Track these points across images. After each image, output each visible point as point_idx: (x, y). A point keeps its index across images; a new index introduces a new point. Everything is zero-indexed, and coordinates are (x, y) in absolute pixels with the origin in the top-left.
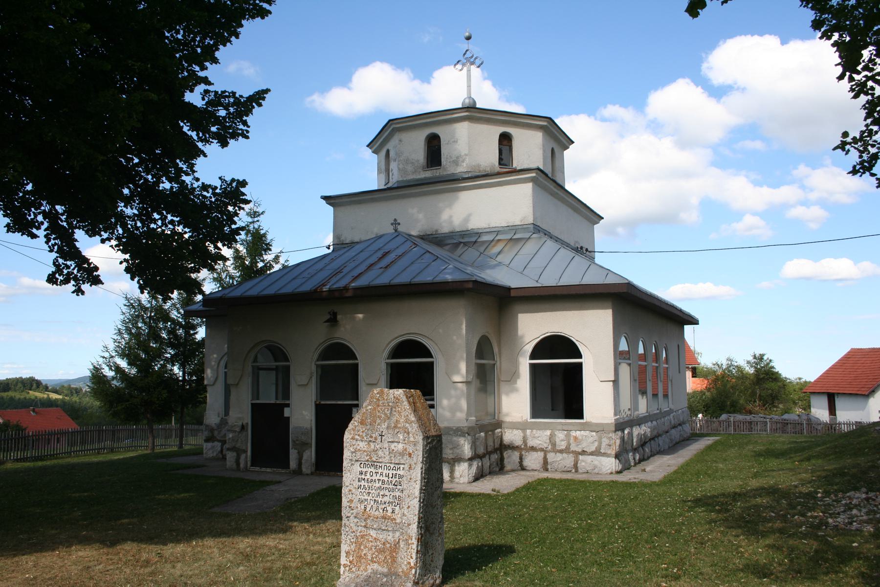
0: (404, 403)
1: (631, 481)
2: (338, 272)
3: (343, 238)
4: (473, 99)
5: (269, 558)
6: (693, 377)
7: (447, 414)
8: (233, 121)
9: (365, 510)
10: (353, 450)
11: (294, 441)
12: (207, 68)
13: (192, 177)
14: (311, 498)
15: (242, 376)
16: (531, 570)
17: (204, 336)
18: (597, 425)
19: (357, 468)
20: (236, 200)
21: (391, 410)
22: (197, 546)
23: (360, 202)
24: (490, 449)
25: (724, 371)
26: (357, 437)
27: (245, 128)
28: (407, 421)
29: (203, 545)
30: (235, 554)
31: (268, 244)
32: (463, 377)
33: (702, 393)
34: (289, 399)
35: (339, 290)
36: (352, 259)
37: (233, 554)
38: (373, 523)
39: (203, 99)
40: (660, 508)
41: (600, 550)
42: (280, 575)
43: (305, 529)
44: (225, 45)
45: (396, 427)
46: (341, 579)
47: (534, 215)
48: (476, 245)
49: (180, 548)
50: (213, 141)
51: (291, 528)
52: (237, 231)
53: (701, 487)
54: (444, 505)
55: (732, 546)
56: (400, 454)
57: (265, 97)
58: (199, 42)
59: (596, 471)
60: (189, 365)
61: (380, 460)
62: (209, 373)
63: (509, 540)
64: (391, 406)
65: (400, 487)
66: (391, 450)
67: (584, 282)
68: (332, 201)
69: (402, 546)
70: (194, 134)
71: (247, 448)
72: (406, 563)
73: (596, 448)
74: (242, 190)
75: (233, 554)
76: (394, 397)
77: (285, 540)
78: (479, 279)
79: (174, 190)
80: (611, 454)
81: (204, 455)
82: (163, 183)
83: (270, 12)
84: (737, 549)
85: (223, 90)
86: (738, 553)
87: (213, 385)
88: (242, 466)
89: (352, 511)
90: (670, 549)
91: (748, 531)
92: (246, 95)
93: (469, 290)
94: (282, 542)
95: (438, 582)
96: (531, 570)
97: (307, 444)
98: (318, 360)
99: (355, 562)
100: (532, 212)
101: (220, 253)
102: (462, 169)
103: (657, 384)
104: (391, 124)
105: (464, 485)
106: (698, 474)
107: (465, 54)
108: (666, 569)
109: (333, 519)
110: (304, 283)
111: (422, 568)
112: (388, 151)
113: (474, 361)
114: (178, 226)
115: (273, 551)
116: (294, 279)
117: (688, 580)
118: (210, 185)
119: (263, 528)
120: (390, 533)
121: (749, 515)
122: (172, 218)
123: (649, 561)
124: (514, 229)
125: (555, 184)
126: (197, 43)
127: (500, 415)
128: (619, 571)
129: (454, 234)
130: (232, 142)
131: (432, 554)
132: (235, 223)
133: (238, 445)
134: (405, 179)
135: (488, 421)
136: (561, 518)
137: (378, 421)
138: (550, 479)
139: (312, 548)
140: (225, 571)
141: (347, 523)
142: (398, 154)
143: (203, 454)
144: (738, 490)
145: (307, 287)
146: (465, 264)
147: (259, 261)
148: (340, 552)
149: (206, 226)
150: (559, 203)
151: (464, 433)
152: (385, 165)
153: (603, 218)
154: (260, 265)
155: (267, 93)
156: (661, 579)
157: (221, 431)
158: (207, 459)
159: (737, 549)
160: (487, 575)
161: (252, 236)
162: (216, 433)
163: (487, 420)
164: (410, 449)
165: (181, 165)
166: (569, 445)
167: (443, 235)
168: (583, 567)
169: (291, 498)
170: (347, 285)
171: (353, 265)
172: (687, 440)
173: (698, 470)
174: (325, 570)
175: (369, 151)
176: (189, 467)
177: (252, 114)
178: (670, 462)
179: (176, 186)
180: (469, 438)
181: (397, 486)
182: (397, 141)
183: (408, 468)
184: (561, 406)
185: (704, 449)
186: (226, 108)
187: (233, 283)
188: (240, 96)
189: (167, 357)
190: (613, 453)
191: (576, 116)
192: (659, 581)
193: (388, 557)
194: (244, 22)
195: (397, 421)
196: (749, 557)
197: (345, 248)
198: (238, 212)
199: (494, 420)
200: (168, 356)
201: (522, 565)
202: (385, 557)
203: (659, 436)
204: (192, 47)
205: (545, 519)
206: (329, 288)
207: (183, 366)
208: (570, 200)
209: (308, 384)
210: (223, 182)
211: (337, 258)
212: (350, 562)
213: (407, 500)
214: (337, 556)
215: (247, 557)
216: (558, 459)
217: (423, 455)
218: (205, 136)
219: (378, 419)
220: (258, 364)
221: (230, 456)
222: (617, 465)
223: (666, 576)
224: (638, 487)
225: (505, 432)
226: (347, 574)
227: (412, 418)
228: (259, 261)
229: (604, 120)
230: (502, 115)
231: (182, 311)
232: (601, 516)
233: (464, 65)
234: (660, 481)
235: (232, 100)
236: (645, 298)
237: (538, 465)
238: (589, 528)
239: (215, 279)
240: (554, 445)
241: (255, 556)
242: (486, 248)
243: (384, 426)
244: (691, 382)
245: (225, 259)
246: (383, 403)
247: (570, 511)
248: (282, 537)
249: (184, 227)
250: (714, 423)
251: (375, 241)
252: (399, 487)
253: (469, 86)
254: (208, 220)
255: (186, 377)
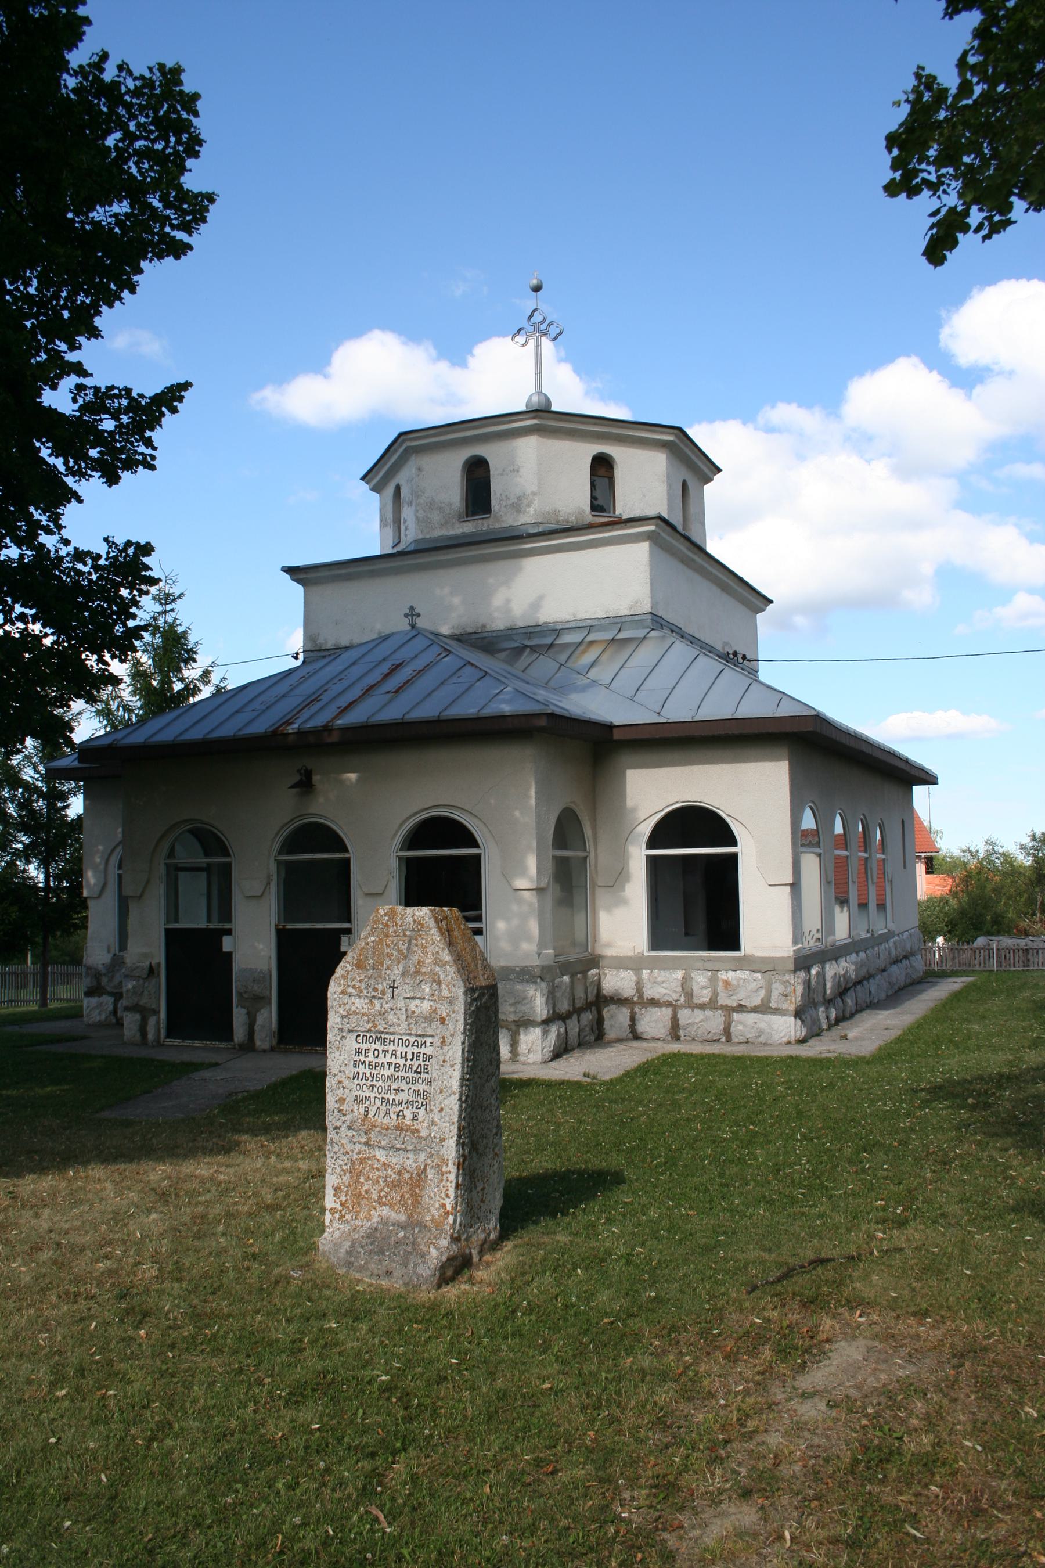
0: (432, 932)
1: (823, 1056)
2: (313, 699)
3: (321, 640)
4: (545, 395)
5: (202, 1199)
6: (927, 873)
7: (505, 945)
8: (127, 439)
9: (366, 1116)
10: (344, 1013)
11: (240, 994)
12: (80, 345)
13: (57, 537)
14: (270, 1093)
15: (147, 883)
16: (653, 1214)
17: (81, 811)
18: (764, 960)
19: (351, 1044)
20: (135, 578)
21: (410, 942)
22: (75, 1178)
23: (348, 578)
24: (578, 1005)
25: (980, 862)
26: (350, 990)
27: (149, 451)
28: (437, 961)
29: (86, 1177)
30: (142, 1191)
31: (191, 650)
32: (532, 881)
33: (943, 901)
34: (230, 921)
35: (316, 732)
36: (338, 677)
37: (139, 1192)
38: (380, 1138)
39: (75, 401)
40: (873, 1102)
41: (770, 1178)
42: (221, 1228)
43: (262, 1146)
44: (111, 306)
45: (417, 972)
46: (326, 1234)
47: (652, 598)
48: (552, 650)
49: (47, 1182)
50: (93, 473)
51: (238, 1146)
52: (136, 633)
53: (943, 1065)
54: (502, 1102)
55: (996, 1166)
56: (425, 1018)
57: (183, 397)
58: (66, 299)
59: (762, 1039)
60: (56, 862)
61: (392, 1030)
62: (91, 878)
63: (614, 1161)
64: (410, 936)
65: (426, 1075)
66: (409, 1013)
67: (739, 715)
68: (302, 576)
69: (430, 1176)
70: (59, 463)
71: (159, 1006)
72: (437, 1205)
73: (762, 1000)
74: (145, 560)
75: (139, 1192)
76: (414, 921)
77: (228, 1166)
78: (558, 711)
79: (26, 561)
80: (787, 1010)
81: (85, 1019)
82: (7, 547)
83: (191, 248)
84: (1004, 1172)
85: (109, 385)
86: (1005, 1179)
87: (99, 897)
88: (151, 1036)
89: (343, 1118)
90: (891, 1174)
91: (1023, 1141)
92: (149, 393)
93: (541, 730)
94: (222, 1169)
95: (493, 1236)
96: (653, 1214)
97: (263, 998)
98: (280, 853)
99: (350, 1204)
100: (649, 592)
101: (107, 670)
102: (527, 518)
103: (867, 886)
104: (404, 441)
105: (535, 1067)
106: (937, 1042)
107: (531, 317)
108: (884, 1209)
109: (310, 1129)
110: (253, 720)
111: (464, 1214)
112: (398, 489)
113: (551, 852)
114: (34, 623)
115: (208, 1185)
116: (237, 712)
117: (922, 1227)
118: (89, 551)
119: (190, 1145)
120: (411, 1155)
121: (1024, 1114)
122: (23, 610)
123: (854, 1194)
124: (618, 622)
125: (688, 544)
126: (62, 302)
127: (596, 945)
128: (803, 1214)
129: (514, 632)
130: (125, 476)
131: (483, 1189)
132: (134, 617)
133: (143, 1001)
134: (428, 537)
135: (575, 956)
136: (703, 1123)
137: (387, 962)
138: (684, 1054)
139: (275, 1179)
140: (126, 1221)
141: (336, 1138)
142: (416, 494)
143: (82, 1016)
144: (1006, 1070)
145: (260, 727)
146: (534, 685)
147: (174, 679)
148: (324, 1187)
149: (83, 623)
150: (697, 578)
151: (534, 977)
152: (394, 512)
153: (771, 602)
154: (178, 686)
155: (186, 390)
156: (876, 1226)
157: (113, 977)
158: (89, 1025)
159: (1004, 1172)
160: (578, 1223)
161: (162, 636)
162: (104, 980)
163: (572, 956)
164: (443, 1011)
165: (37, 515)
166: (715, 994)
167: (494, 634)
168: (742, 1207)
169: (236, 1093)
170: (329, 722)
171: (339, 687)
172: (919, 983)
173: (937, 1036)
174: (298, 1218)
175: (365, 487)
176: (59, 1039)
177: (161, 426)
178: (889, 1022)
179: (30, 553)
180: (544, 985)
181: (420, 1073)
182: (414, 470)
183: (439, 1043)
184: (701, 927)
185: (947, 998)
186: (115, 416)
187: (130, 719)
188: (138, 395)
189: (16, 849)
190: (792, 1008)
191: (722, 423)
192: (872, 1230)
193: (407, 1196)
194: (144, 264)
195: (419, 962)
196: (1024, 1186)
197: (324, 657)
198: (138, 599)
199: (586, 954)
200: (20, 846)
201: (636, 1205)
202: (402, 1196)
203: (870, 976)
204: (54, 308)
205: (675, 1124)
206: (299, 728)
207: (45, 864)
208: (714, 571)
209: (262, 895)
210: (110, 547)
211: (311, 675)
212: (341, 1205)
213: (439, 1098)
214: (319, 1193)
215: (163, 1196)
216: (697, 1020)
217: (465, 1019)
218: (80, 466)
219: (387, 959)
220: (176, 861)
221: (131, 1021)
222: (798, 1028)
223: (884, 1221)
224: (834, 1067)
225: (605, 975)
226: (336, 1225)
227: (446, 956)
228: (174, 679)
229: (770, 430)
230: (595, 424)
231: (41, 768)
232: (772, 1117)
233: (529, 336)
234: (873, 1056)
235: (125, 402)
236: (844, 740)
237: (662, 1031)
238: (751, 1140)
239: (98, 713)
240: (689, 995)
241: (177, 1195)
242: (570, 656)
243: (398, 970)
244: (924, 882)
245: (115, 681)
246: (395, 932)
247: (719, 1110)
248: (222, 1160)
249: (44, 626)
250: (964, 952)
251: (376, 646)
252: (423, 1075)
253: (538, 373)
254: (86, 614)
255: (52, 884)
